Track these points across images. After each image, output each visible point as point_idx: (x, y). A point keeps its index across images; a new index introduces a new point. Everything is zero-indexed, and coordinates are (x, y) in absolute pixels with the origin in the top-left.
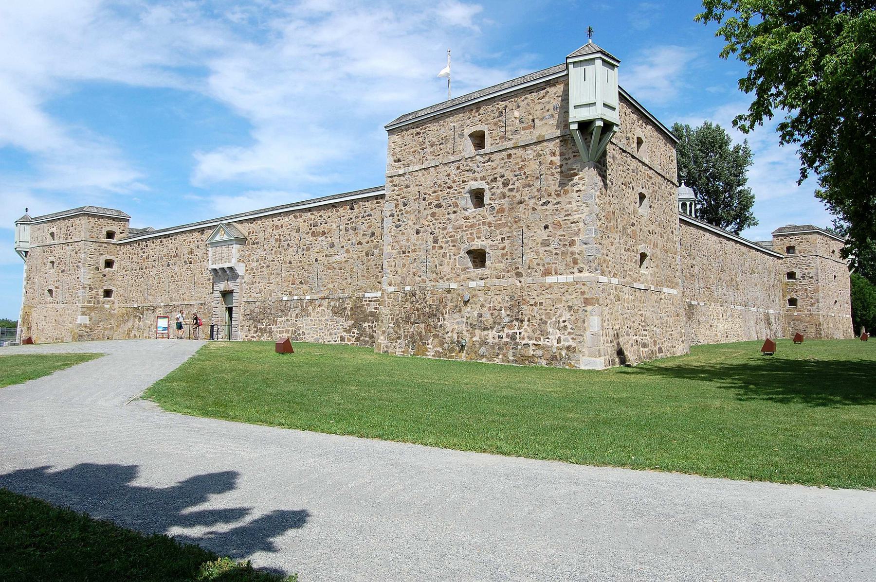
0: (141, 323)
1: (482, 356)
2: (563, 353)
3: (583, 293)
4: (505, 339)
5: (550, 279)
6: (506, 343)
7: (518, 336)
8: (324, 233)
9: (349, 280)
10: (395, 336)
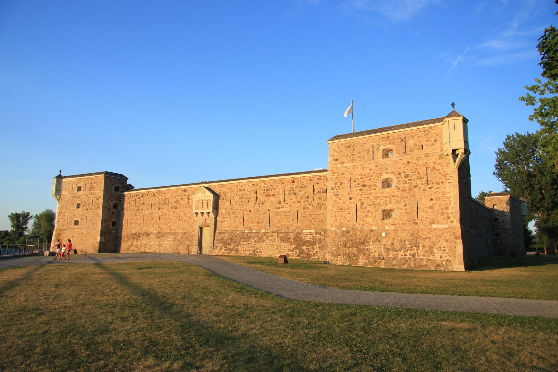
0: (138, 243)
1: (395, 265)
2: (444, 263)
3: (454, 233)
4: (409, 256)
5: (434, 226)
6: (409, 258)
7: (416, 254)
8: (274, 195)
9: (292, 222)
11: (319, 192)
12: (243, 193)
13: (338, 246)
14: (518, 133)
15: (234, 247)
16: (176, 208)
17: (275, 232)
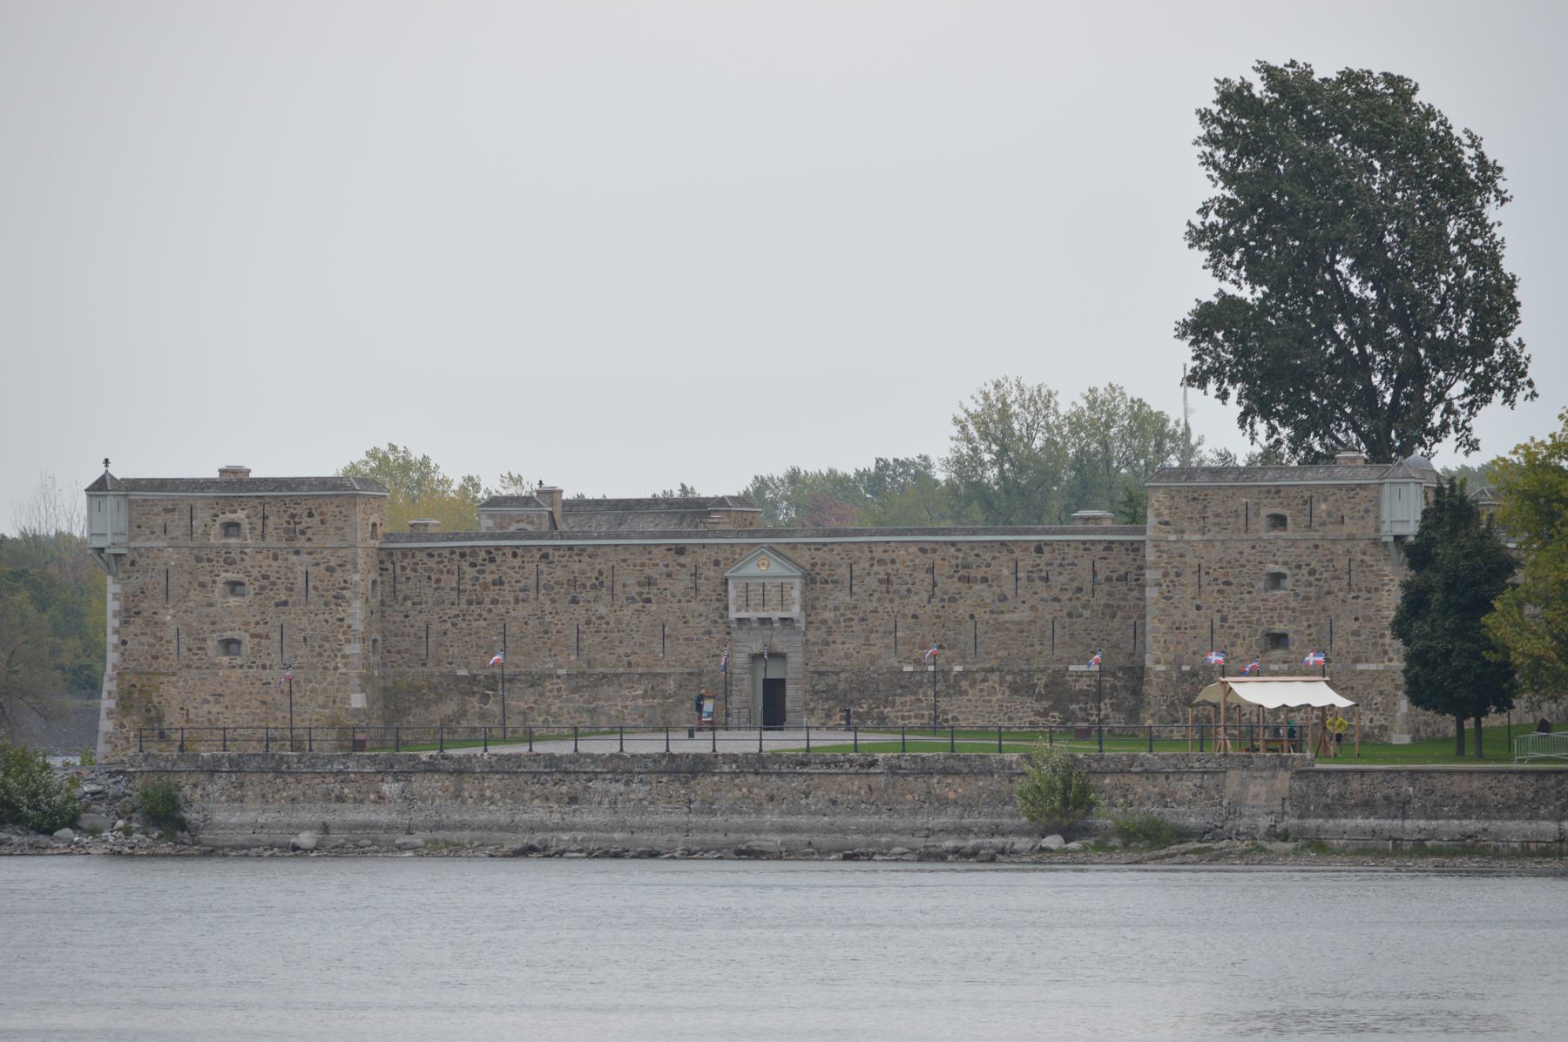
5: (1360, 667)
9: (1038, 648)
10: (1169, 719)
11: (1108, 579)
12: (889, 568)
13: (1172, 703)
14: (1278, 62)
15: (870, 708)
16: (648, 601)
17: (992, 670)
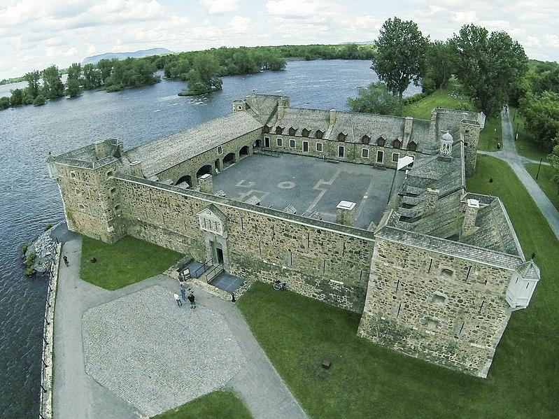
5: (472, 344)
